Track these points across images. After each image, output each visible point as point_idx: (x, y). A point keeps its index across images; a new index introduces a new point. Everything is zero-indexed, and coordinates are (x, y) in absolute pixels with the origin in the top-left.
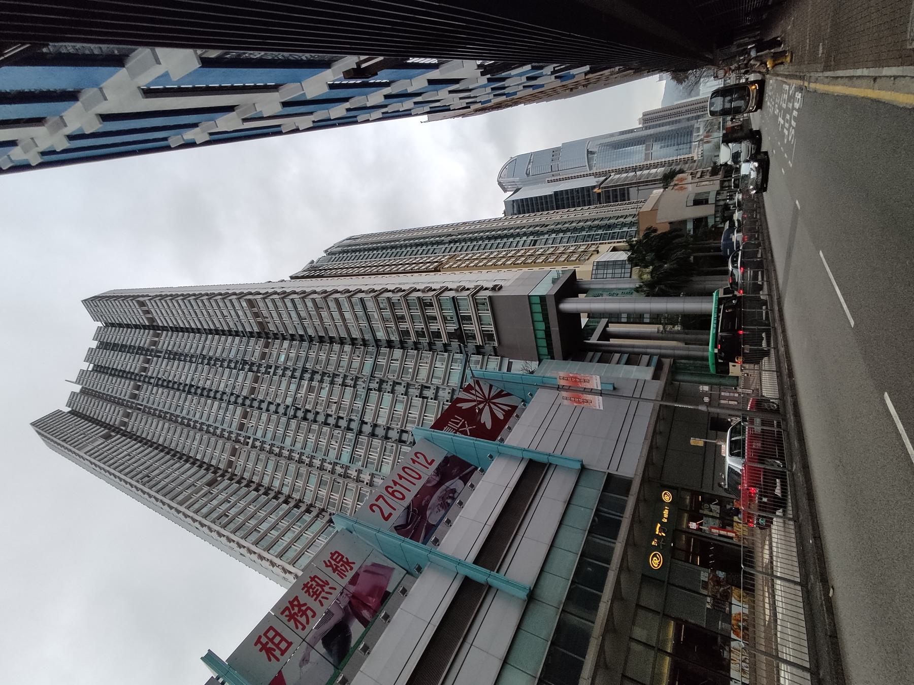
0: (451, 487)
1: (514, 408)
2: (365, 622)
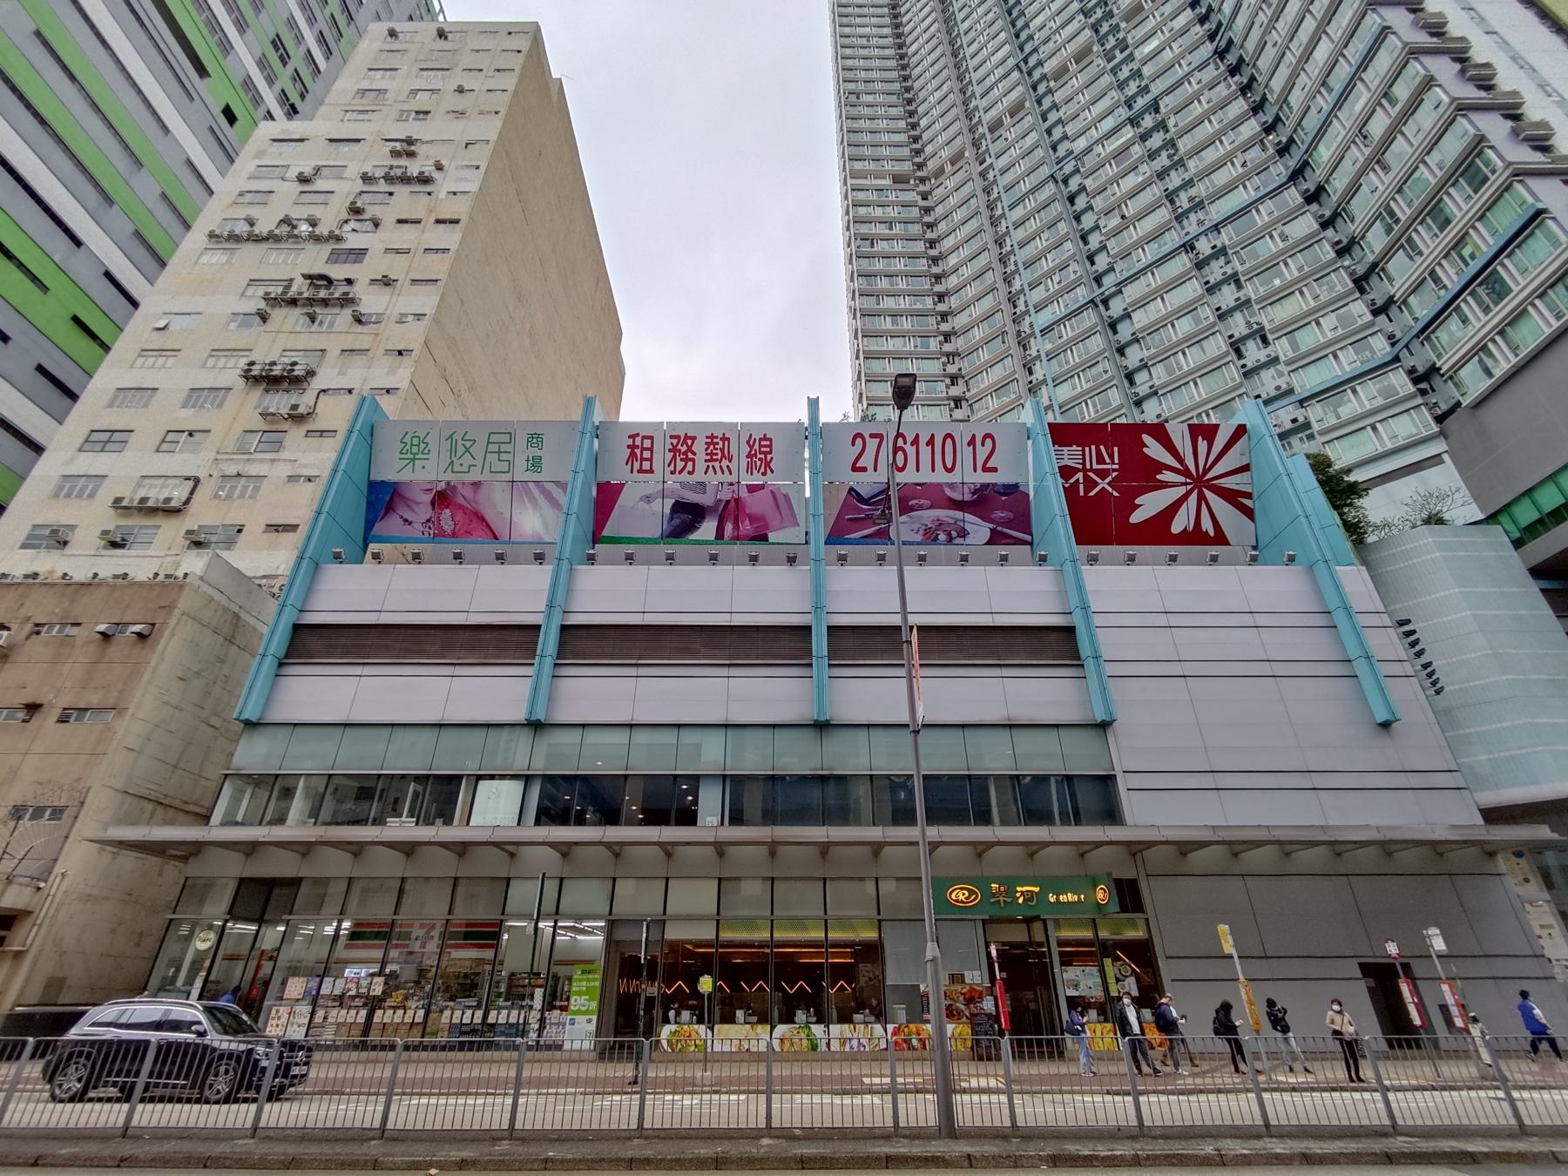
1: (1220, 539)
2: (720, 535)
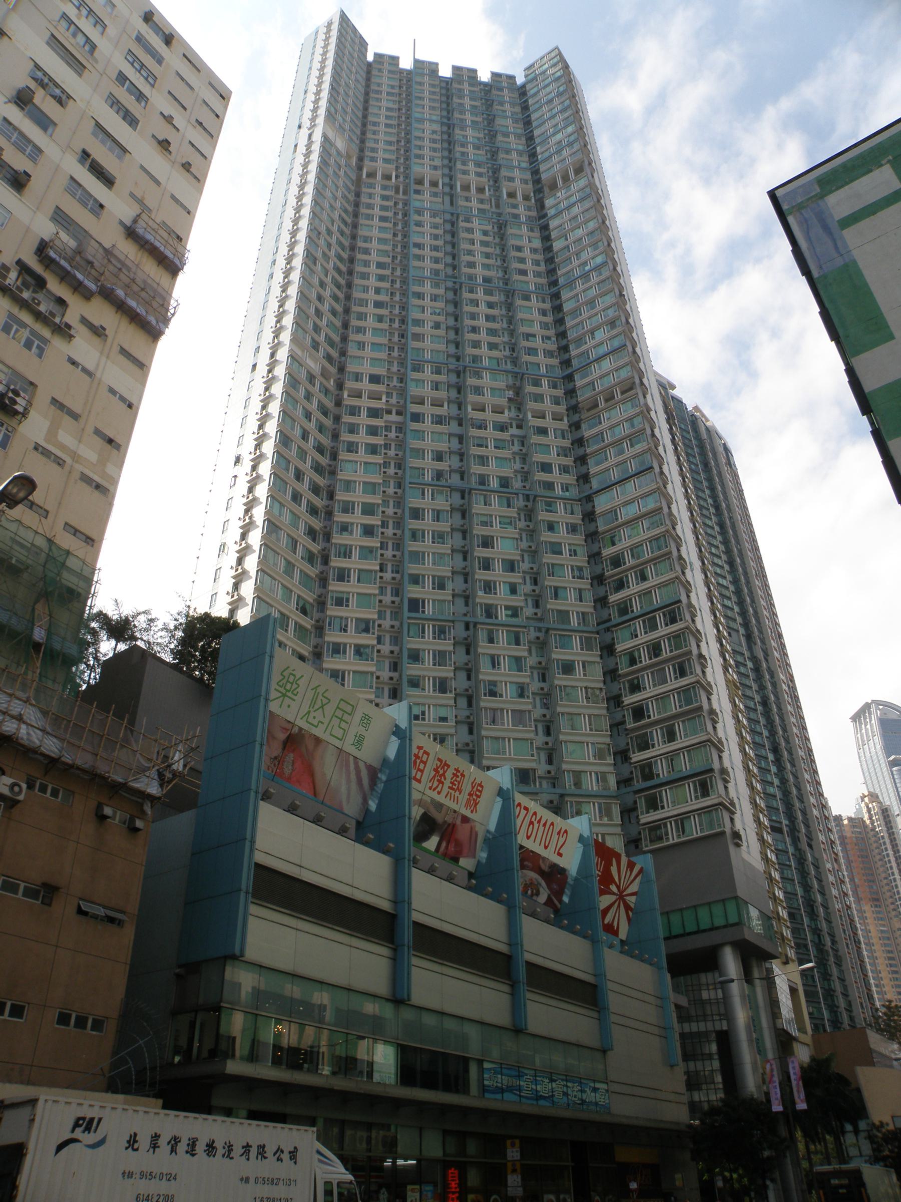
0: (541, 889)
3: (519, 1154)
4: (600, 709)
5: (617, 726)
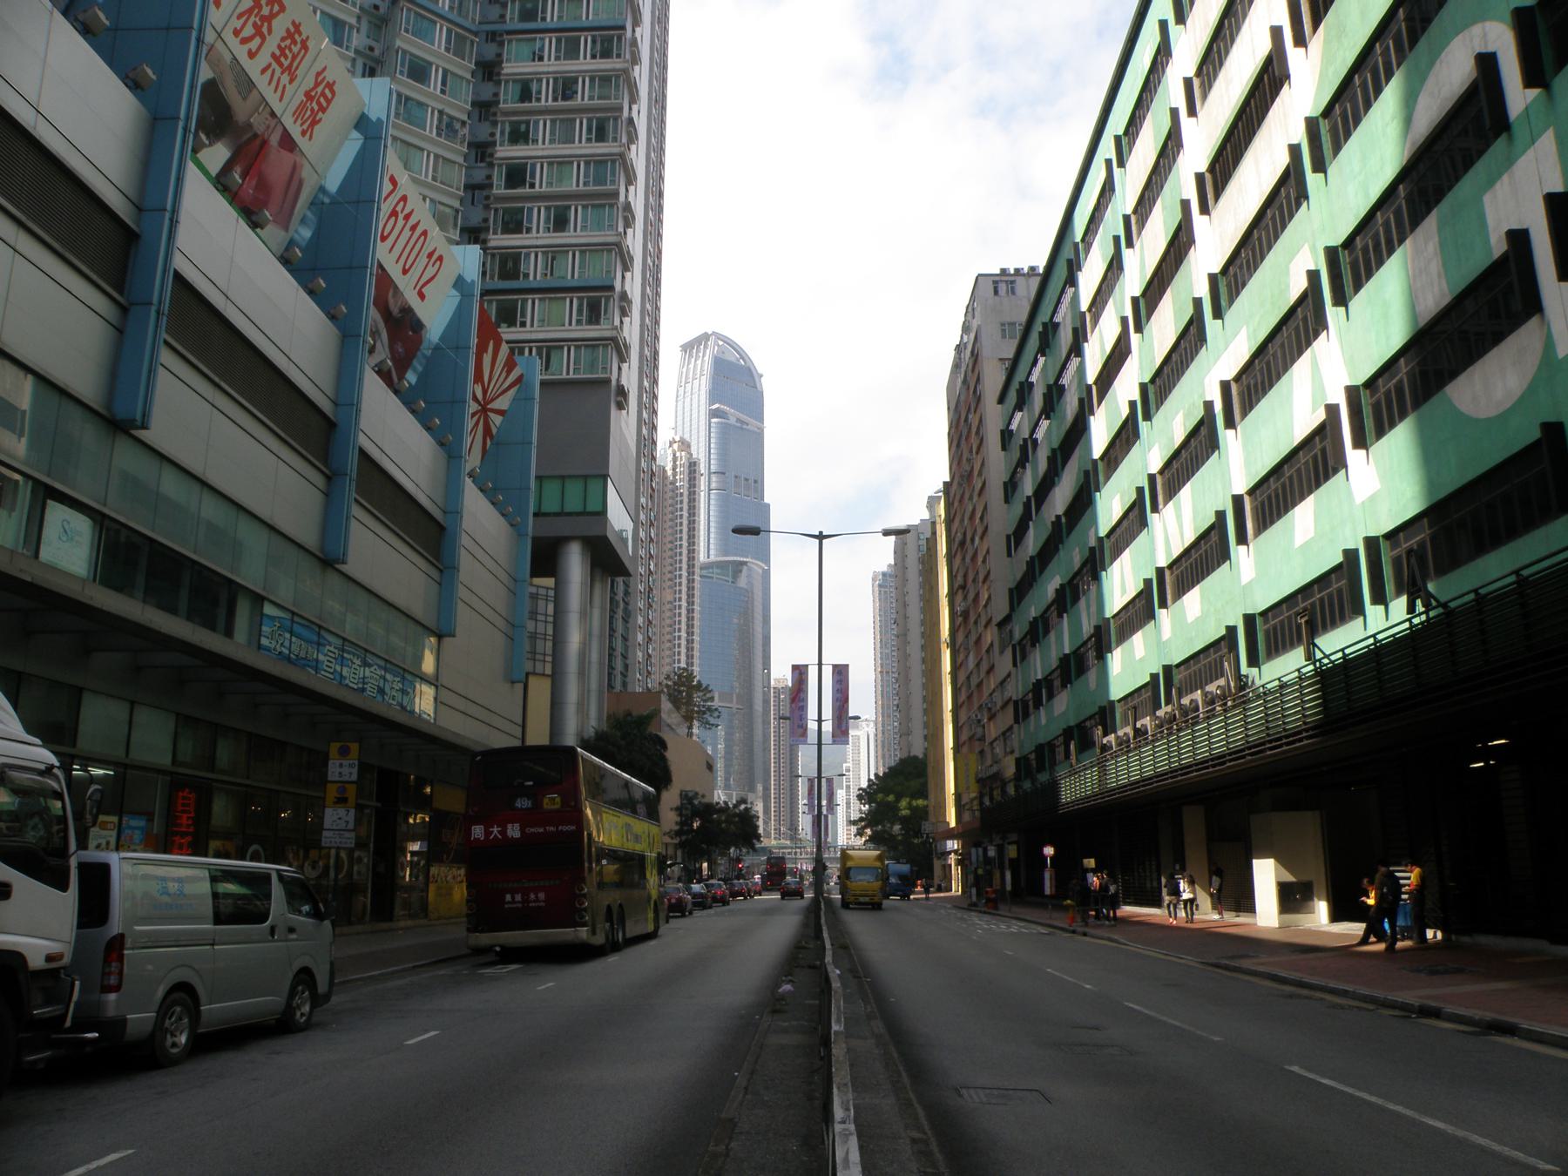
3: (355, 771)
4: (456, 151)
5: (476, 189)
